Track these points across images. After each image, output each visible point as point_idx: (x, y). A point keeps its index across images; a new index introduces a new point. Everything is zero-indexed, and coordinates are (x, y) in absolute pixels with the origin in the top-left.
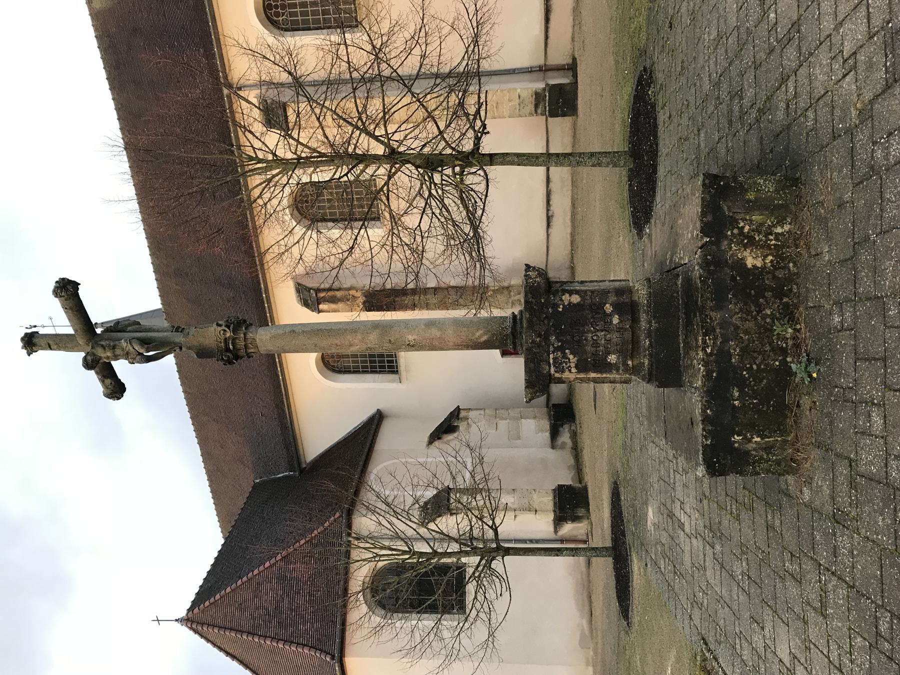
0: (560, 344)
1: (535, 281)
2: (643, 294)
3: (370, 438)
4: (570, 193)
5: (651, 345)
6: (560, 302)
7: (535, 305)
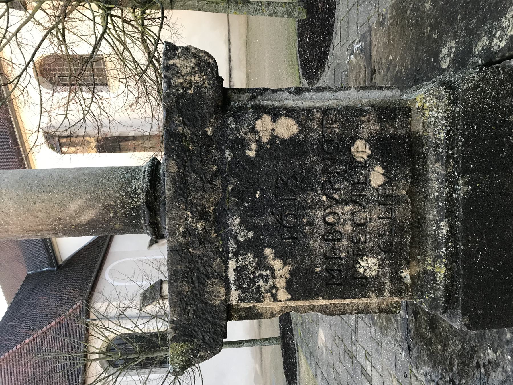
0: (251, 234)
1: (190, 82)
2: (437, 118)
3: (106, 244)
4: (245, 69)
5: (452, 233)
6: (250, 136)
7: (192, 142)
